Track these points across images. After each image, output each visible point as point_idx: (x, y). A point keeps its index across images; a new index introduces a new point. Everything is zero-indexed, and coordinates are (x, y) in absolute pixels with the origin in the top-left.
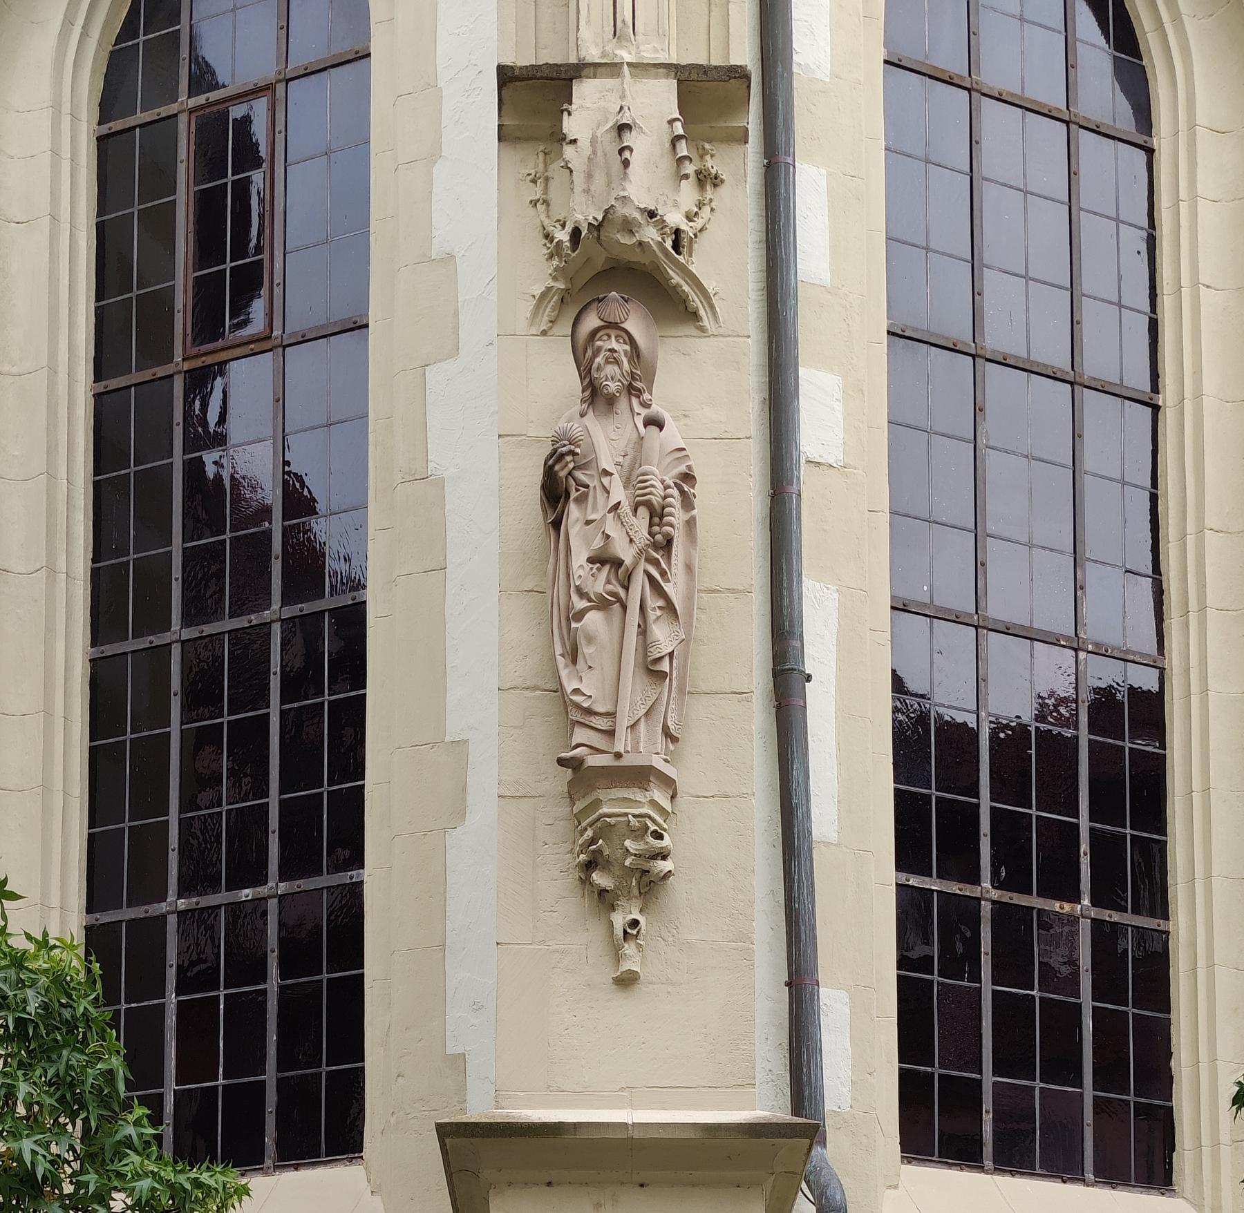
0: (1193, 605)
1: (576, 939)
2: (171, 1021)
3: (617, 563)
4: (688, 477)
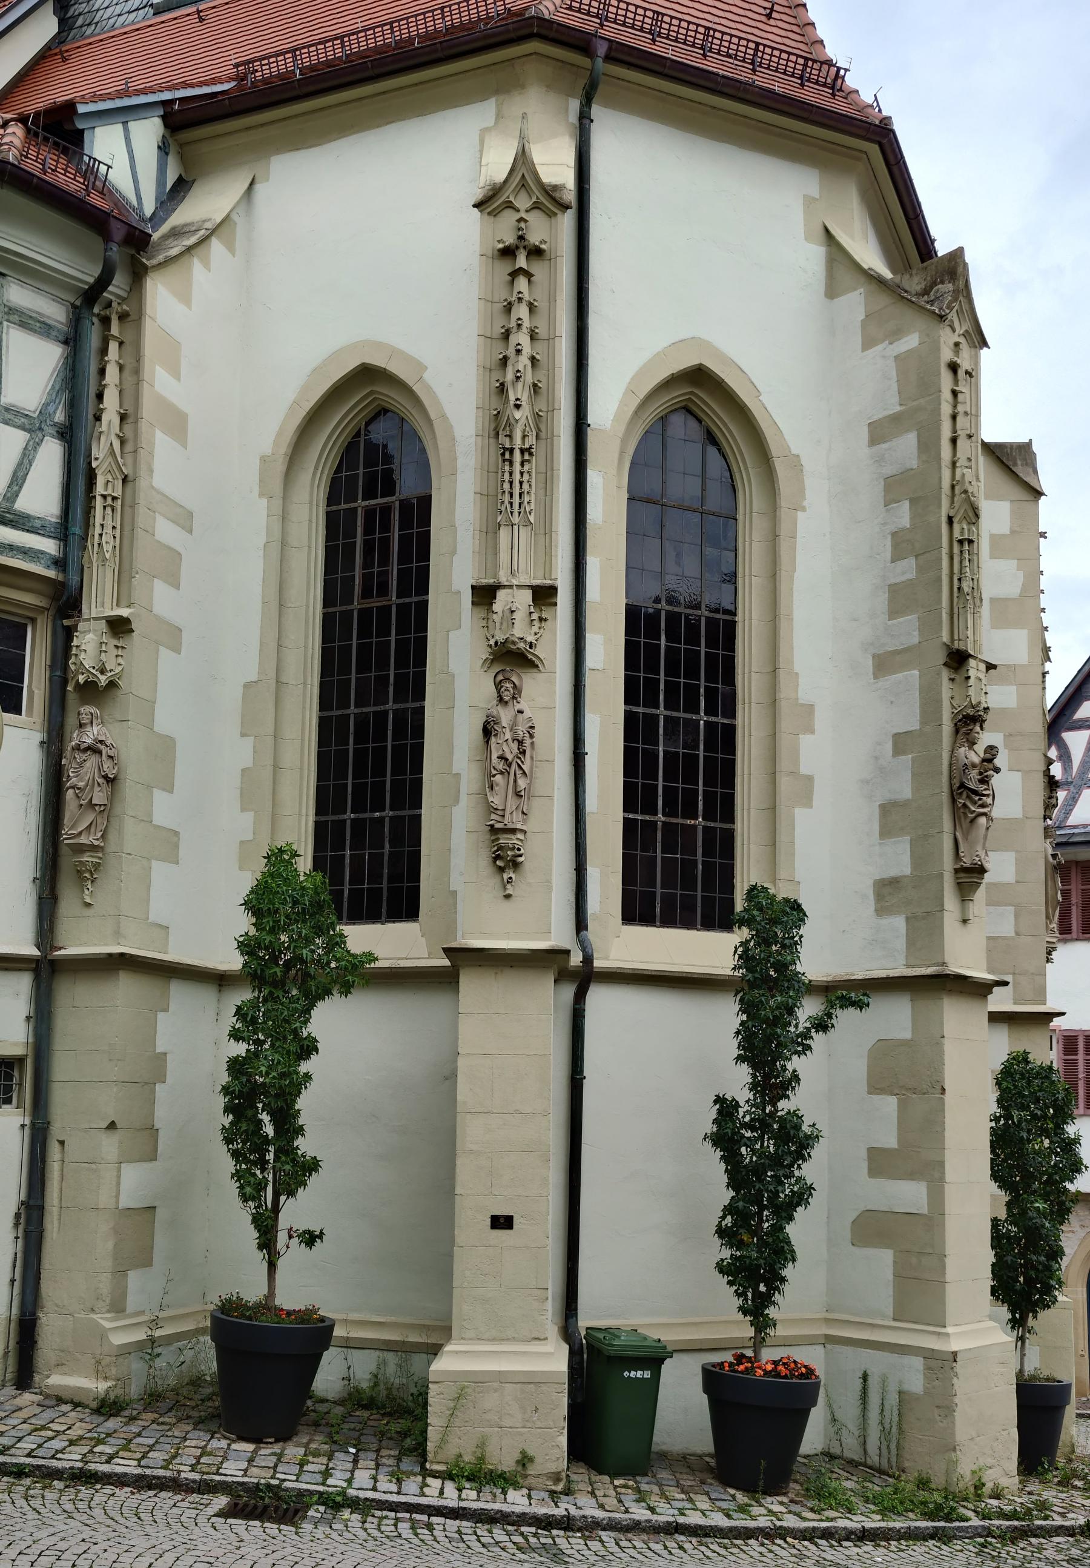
0: (747, 701)
1: (492, 882)
2: (347, 861)
3: (507, 760)
4: (532, 727)
